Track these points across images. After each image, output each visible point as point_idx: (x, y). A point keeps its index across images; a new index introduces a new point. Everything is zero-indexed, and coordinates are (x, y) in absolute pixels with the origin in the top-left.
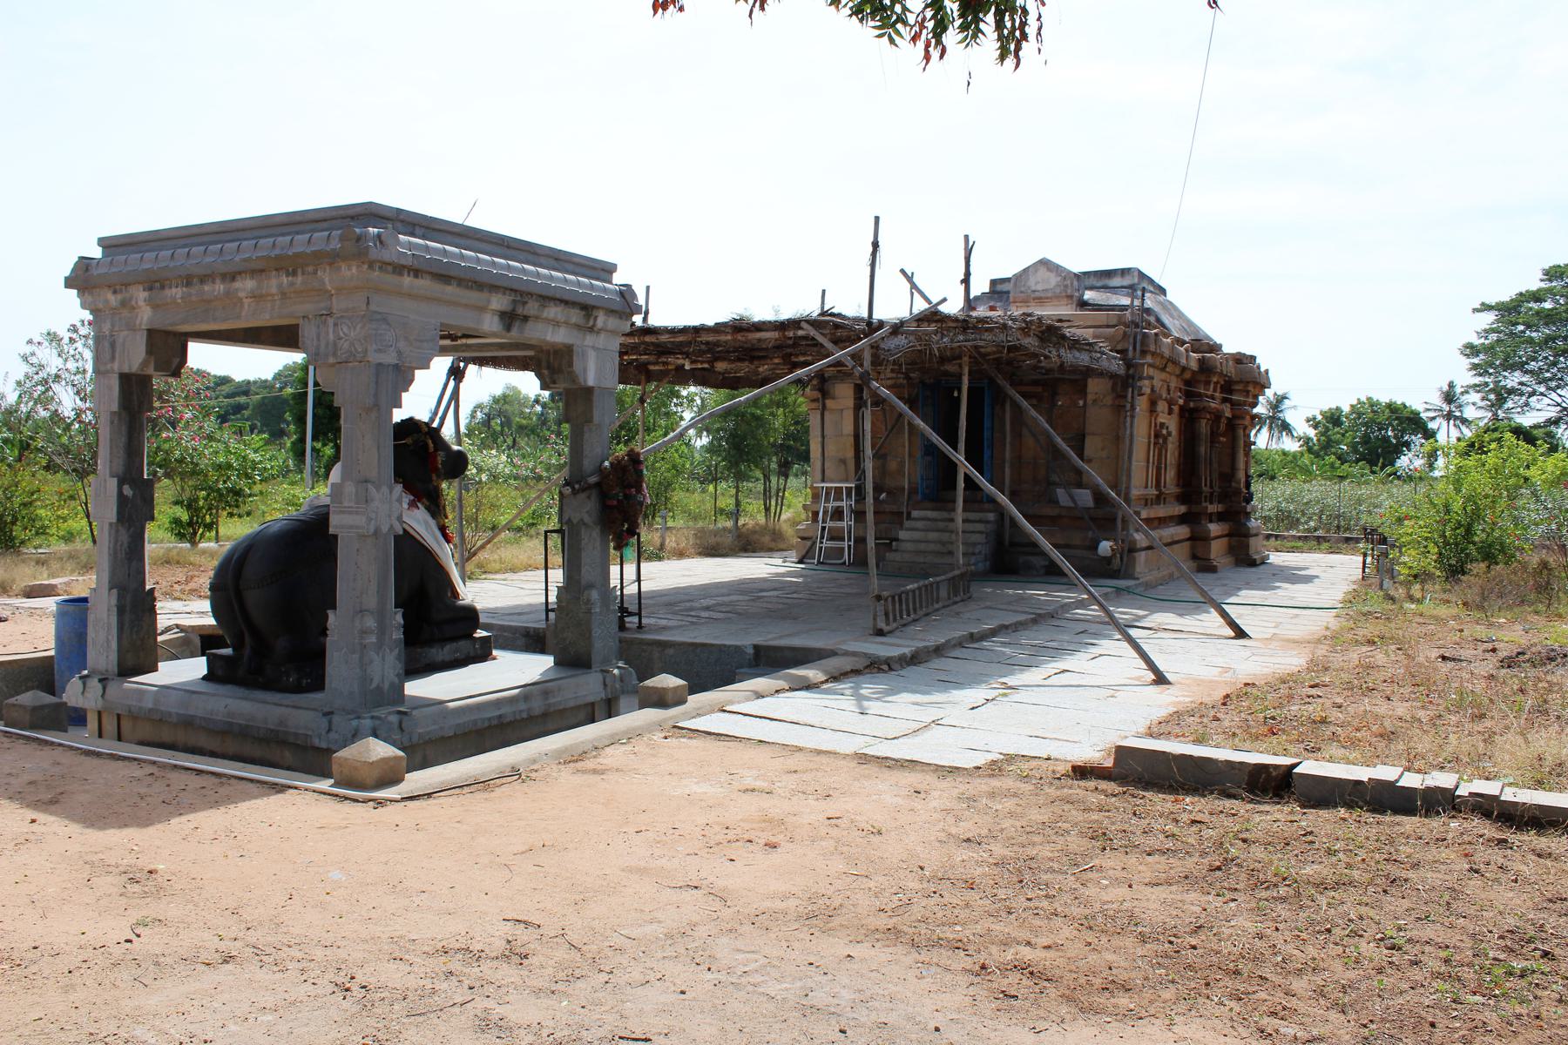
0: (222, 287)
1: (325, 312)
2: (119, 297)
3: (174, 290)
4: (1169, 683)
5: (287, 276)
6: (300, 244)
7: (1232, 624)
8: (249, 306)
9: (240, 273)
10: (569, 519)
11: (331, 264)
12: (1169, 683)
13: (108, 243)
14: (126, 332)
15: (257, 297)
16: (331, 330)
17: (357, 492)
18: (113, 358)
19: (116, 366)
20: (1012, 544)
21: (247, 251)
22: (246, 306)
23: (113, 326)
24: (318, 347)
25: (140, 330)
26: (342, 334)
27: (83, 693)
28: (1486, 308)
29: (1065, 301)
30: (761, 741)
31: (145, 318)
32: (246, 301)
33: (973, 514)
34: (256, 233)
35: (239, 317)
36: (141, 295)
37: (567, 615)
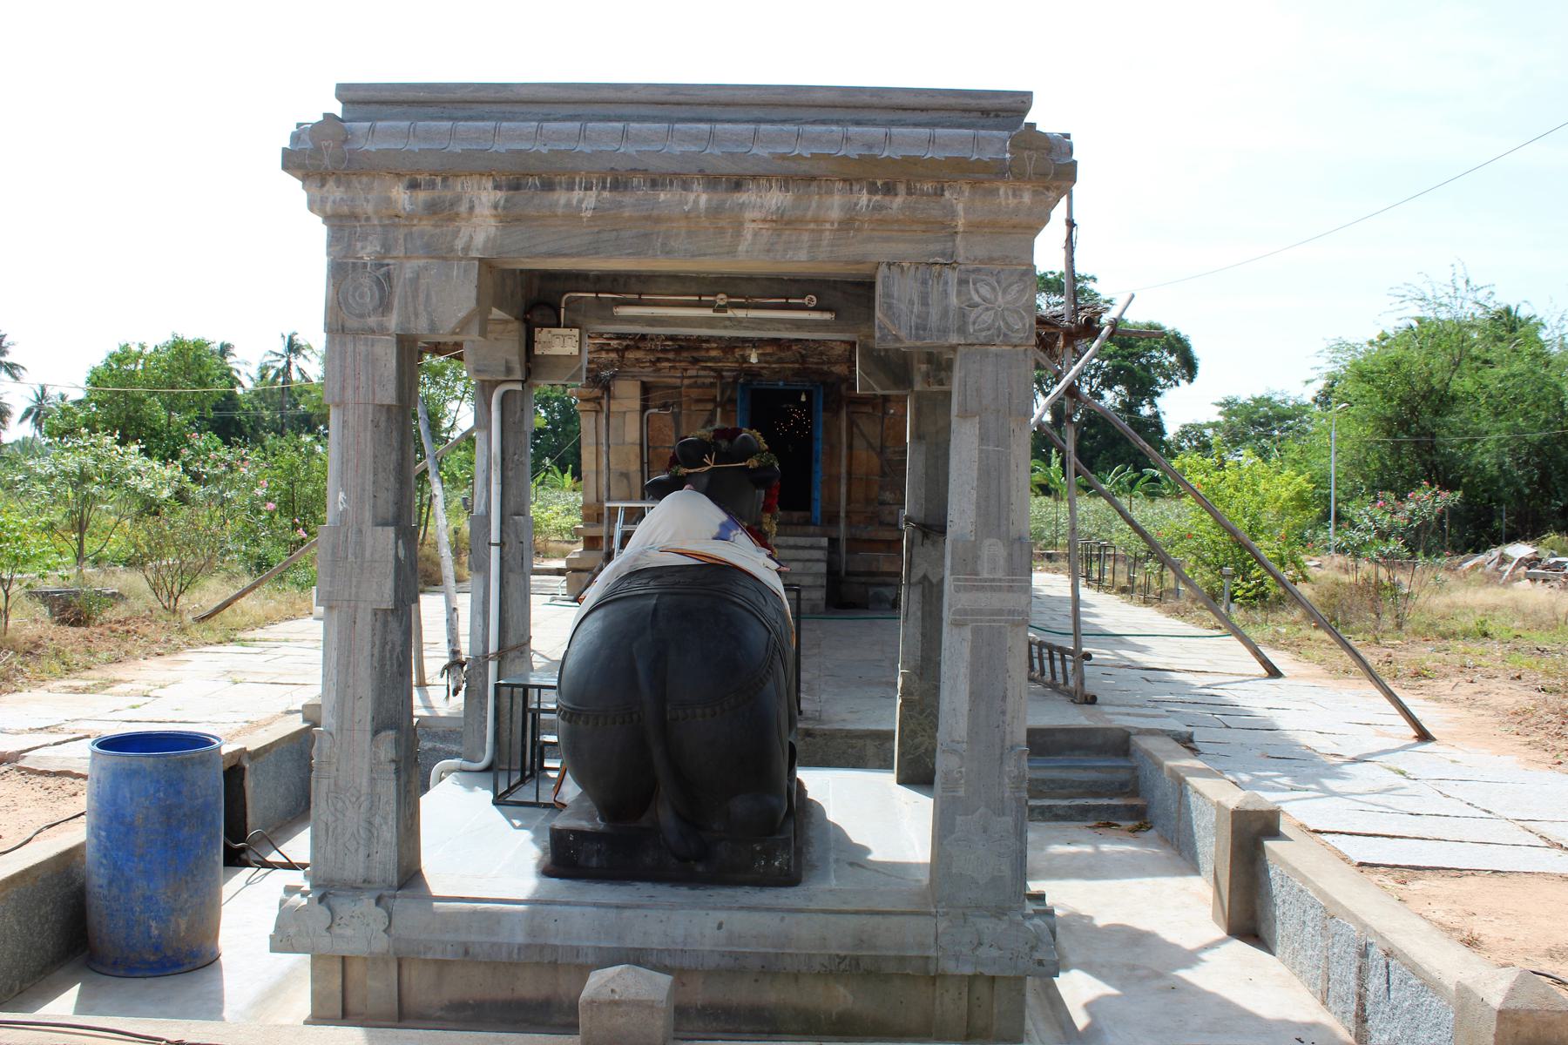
0: (704, 198)
1: (941, 260)
2: (422, 196)
3: (577, 194)
4: (1434, 739)
5: (870, 192)
6: (909, 141)
7: (1266, 663)
8: (756, 234)
9: (754, 177)
10: (925, 577)
11: (975, 184)
12: (1434, 739)
13: (350, 95)
14: (422, 262)
15: (782, 222)
16: (953, 290)
17: (1010, 555)
18: (384, 306)
19: (393, 322)
20: (848, 573)
21: (826, 139)
22: (749, 236)
23: (387, 248)
24: (924, 317)
25: (466, 257)
26: (976, 298)
27: (329, 928)
30: (1495, 872)
31: (480, 239)
32: (749, 228)
33: (803, 539)
34: (757, 113)
35: (732, 252)
36: (485, 197)
37: (922, 711)
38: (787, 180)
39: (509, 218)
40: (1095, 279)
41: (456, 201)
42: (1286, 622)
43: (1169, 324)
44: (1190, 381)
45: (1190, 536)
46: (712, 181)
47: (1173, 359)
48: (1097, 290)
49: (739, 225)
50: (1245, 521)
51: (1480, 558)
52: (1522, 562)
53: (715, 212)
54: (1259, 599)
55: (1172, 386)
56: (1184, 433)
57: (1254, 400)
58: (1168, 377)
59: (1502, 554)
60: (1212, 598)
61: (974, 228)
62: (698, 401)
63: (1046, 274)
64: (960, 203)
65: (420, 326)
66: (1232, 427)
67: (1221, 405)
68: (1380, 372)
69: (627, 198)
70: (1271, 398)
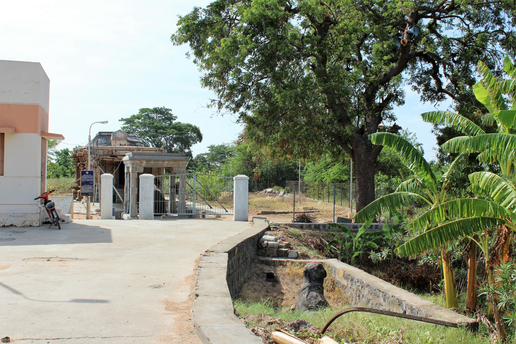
15: (167, 164)
18: (136, 170)
19: (137, 171)
38: (168, 161)
39: (146, 164)
42: (216, 203)
43: (193, 124)
46: (162, 161)
47: (195, 135)
52: (268, 192)
54: (212, 199)
56: (198, 157)
58: (194, 141)
60: (204, 199)
64: (181, 162)
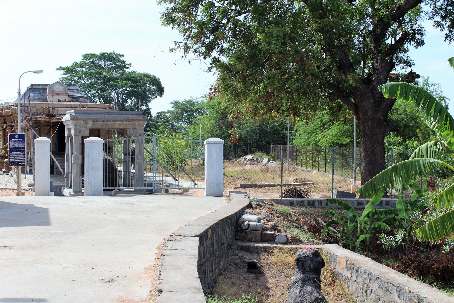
12: (64, 195)
15: (120, 125)
18: (80, 133)
19: (81, 135)
28: (61, 68)
29: (65, 95)
31: (90, 126)
36: (91, 123)
38: (120, 121)
39: (93, 124)
40: (123, 56)
41: (88, 123)
42: (182, 174)
43: (152, 73)
44: (161, 96)
45: (161, 155)
46: (113, 121)
47: (154, 87)
48: (124, 60)
49: (115, 125)
50: (173, 151)
51: (240, 160)
53: (113, 124)
55: (154, 98)
56: (159, 115)
57: (186, 102)
58: (153, 95)
59: (245, 158)
61: (138, 125)
62: (46, 126)
63: (104, 53)
64: (137, 123)
65: (84, 135)
66: (177, 113)
67: (173, 103)
68: (215, 105)
69: (105, 122)
70: (192, 101)
